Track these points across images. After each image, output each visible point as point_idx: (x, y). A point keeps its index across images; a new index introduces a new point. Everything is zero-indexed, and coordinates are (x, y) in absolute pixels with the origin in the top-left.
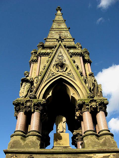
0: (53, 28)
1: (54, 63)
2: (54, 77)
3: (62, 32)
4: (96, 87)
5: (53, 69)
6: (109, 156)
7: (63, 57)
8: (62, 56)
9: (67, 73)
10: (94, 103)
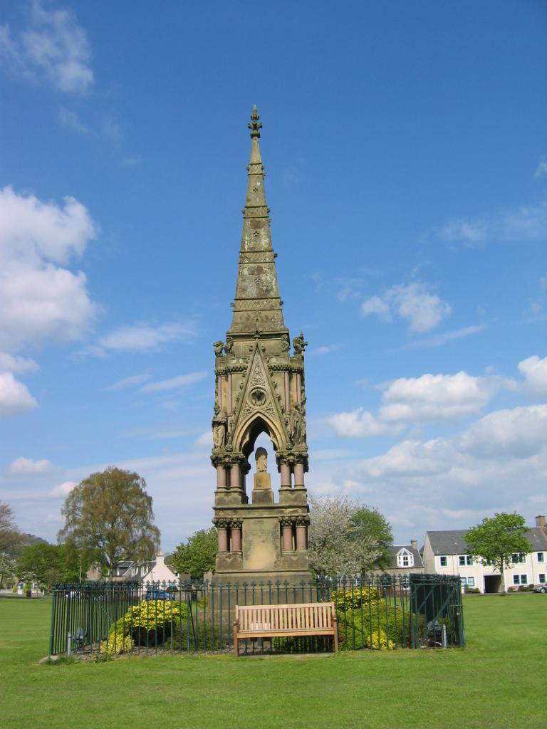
2: (250, 415)
10: (291, 457)
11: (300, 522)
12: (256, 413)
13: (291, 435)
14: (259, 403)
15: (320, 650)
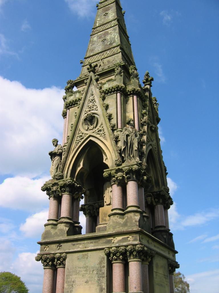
0: (97, 28)
1: (83, 116)
2: (83, 140)
3: (107, 33)
4: (129, 145)
5: (82, 129)
6: (128, 237)
7: (95, 101)
8: (93, 100)
9: (97, 131)
10: (120, 174)
11: (131, 253)
13: (120, 150)
14: (91, 127)
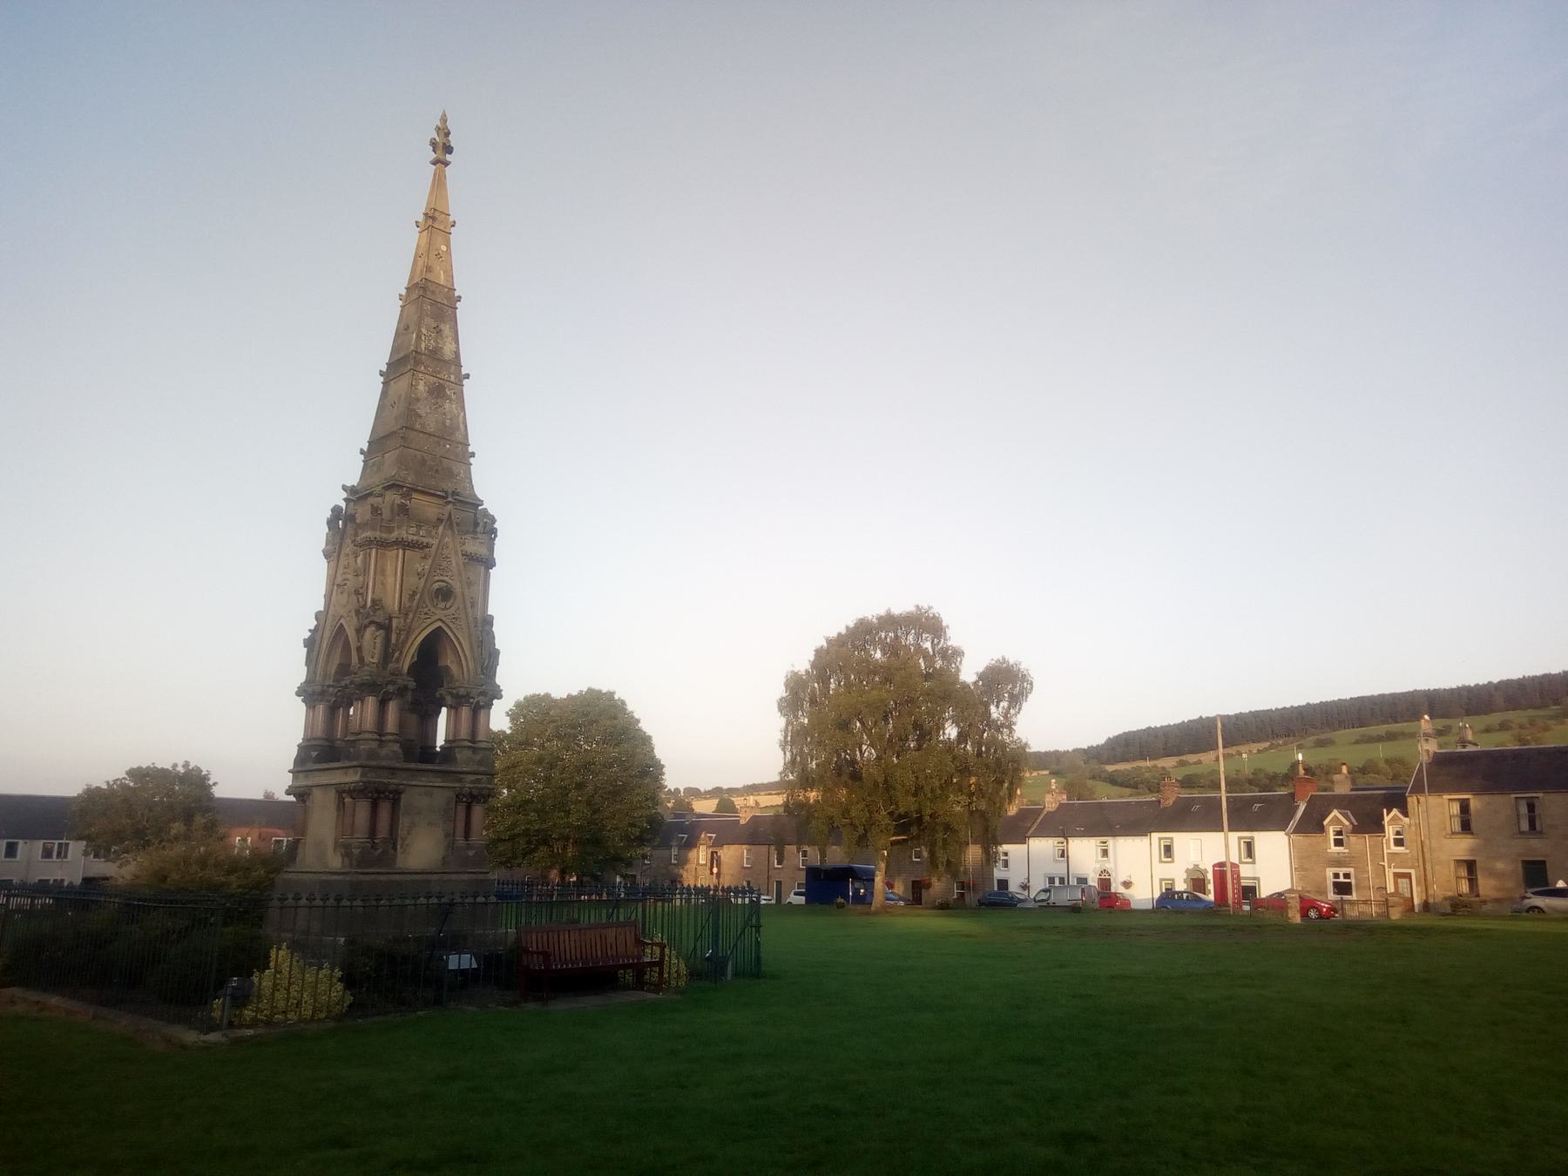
12: (437, 620)
14: (442, 605)
15: (1534, 821)
